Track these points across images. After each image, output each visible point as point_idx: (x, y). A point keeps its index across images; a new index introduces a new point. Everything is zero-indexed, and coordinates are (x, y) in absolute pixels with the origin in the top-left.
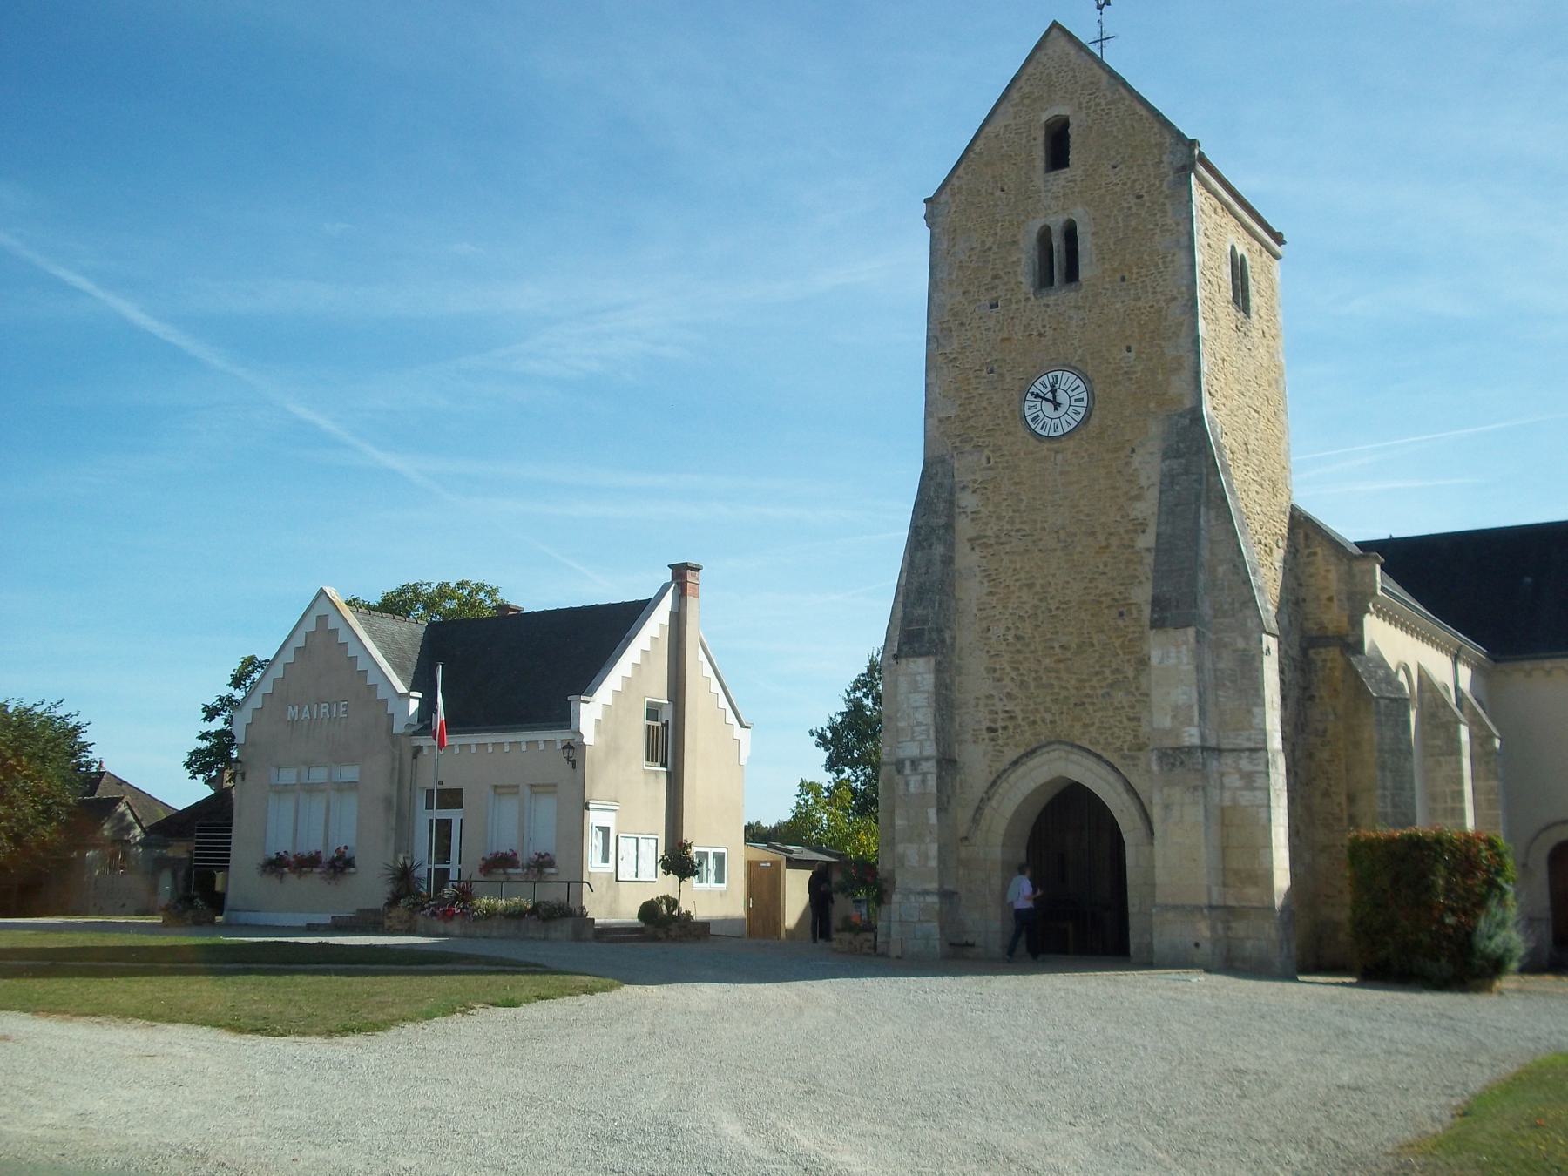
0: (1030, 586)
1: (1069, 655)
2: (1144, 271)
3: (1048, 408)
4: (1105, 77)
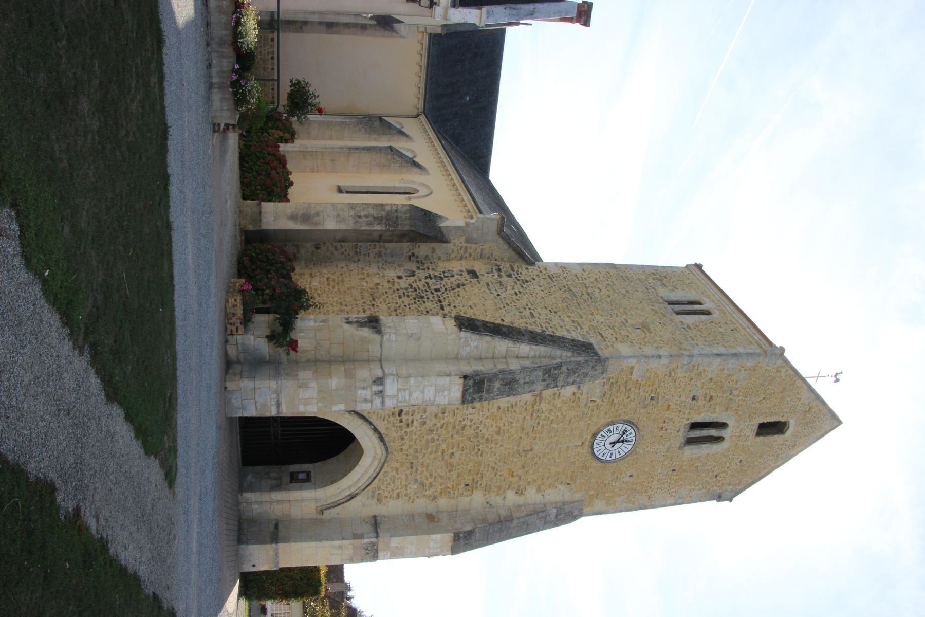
0: (498, 433)
1: (446, 457)
2: (673, 482)
3: (614, 438)
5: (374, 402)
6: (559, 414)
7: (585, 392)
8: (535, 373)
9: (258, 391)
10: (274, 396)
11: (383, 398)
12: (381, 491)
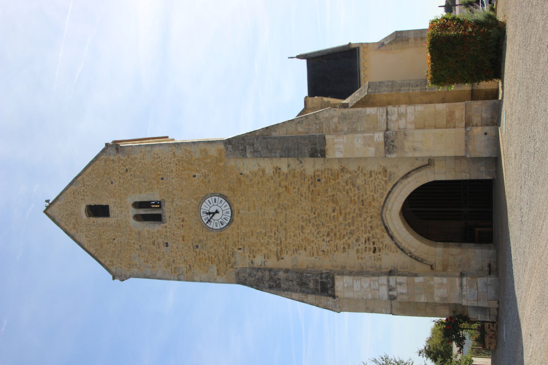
0: (303, 228)
1: (338, 208)
2: (160, 168)
3: (217, 216)
5: (394, 283)
6: (261, 240)
7: (247, 258)
8: (286, 287)
9: (475, 298)
10: (464, 293)
11: (389, 285)
12: (385, 179)
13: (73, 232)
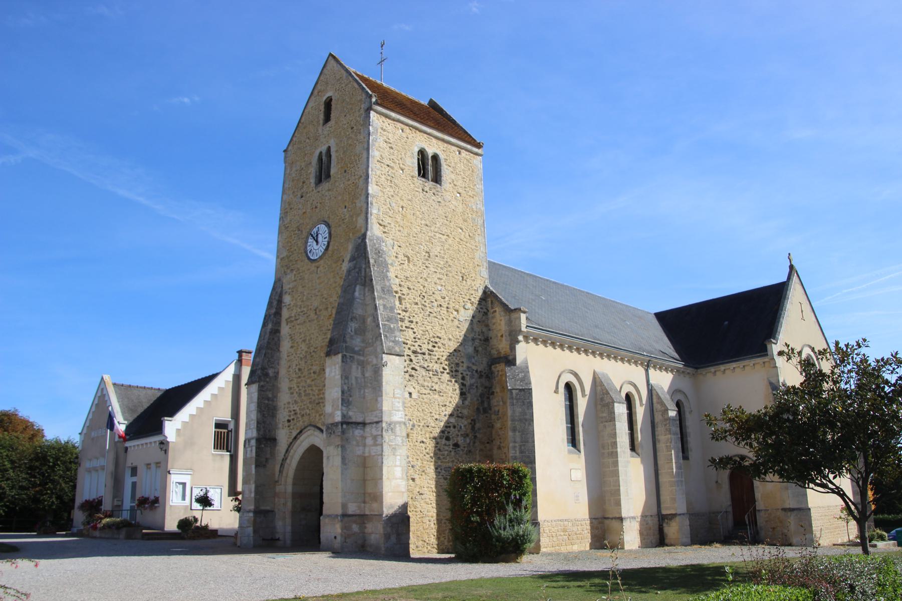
0: (304, 341)
4: (345, 73)
13: (316, 92)
